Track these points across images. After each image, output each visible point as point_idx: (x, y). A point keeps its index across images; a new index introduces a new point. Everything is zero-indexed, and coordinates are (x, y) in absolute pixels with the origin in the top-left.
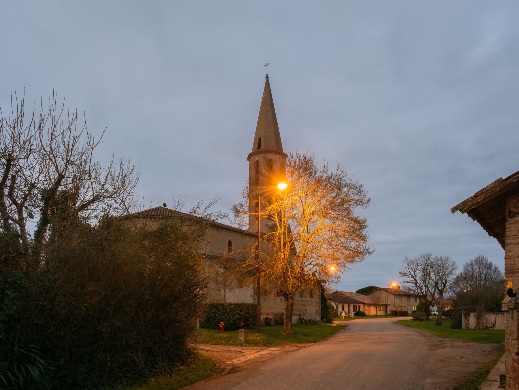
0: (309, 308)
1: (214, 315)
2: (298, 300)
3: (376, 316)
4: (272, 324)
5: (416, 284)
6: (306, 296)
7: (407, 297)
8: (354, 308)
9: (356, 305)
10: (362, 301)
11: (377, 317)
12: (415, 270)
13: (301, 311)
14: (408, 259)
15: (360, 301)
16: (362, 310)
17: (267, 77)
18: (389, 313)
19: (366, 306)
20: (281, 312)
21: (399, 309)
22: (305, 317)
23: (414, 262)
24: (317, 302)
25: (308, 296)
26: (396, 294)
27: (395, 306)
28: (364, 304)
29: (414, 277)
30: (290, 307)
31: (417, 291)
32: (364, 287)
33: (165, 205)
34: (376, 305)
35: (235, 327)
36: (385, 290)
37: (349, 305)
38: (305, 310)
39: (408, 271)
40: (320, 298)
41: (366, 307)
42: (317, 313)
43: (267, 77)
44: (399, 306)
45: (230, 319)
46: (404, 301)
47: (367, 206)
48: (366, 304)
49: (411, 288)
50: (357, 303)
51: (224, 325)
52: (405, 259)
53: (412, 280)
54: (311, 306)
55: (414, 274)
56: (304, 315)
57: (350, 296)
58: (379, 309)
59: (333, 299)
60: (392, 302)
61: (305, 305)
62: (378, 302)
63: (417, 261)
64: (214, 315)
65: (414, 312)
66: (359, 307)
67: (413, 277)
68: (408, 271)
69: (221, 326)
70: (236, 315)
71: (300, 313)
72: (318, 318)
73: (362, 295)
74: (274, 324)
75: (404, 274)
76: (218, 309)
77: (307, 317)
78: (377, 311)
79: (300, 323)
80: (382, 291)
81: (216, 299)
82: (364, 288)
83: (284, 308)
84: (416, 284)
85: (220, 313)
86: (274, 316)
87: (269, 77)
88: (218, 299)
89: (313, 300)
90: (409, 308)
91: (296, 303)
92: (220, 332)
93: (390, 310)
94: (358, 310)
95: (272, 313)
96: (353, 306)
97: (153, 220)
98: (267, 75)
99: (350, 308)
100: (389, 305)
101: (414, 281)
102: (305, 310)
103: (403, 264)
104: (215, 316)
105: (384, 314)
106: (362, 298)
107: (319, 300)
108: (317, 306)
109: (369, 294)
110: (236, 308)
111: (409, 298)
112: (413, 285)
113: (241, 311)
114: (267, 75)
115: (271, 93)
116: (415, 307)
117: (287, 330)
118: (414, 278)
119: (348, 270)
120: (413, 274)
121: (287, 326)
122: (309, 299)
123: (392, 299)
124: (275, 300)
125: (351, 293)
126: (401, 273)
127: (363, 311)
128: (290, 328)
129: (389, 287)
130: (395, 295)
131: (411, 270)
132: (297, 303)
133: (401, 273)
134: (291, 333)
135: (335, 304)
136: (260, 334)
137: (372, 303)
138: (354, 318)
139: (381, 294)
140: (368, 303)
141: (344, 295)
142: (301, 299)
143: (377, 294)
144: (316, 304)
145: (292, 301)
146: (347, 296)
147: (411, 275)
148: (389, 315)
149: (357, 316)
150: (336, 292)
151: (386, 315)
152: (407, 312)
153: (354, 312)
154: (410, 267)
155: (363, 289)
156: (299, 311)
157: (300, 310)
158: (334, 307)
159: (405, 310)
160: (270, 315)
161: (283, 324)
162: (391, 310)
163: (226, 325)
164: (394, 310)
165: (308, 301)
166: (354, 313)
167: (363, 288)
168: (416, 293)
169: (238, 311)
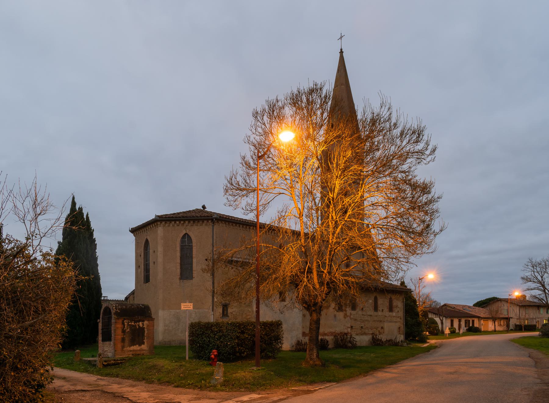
0: (386, 325)
1: (209, 339)
2: (371, 316)
3: (495, 332)
4: (330, 346)
5: (544, 291)
6: (382, 310)
7: (535, 308)
8: (466, 323)
9: (469, 319)
10: (476, 314)
11: (496, 333)
12: (543, 273)
13: (375, 330)
14: (534, 260)
15: (475, 314)
16: (476, 325)
17: (341, 52)
18: (511, 327)
19: (482, 321)
20: (346, 331)
21: (525, 322)
22: (379, 337)
23: (540, 264)
24: (399, 317)
25: (386, 309)
26: (521, 305)
27: (519, 318)
28: (479, 318)
29: (541, 282)
30: (314, 324)
31: (546, 301)
32: (483, 298)
33: (204, 207)
34: (494, 319)
35: (234, 357)
36: (506, 301)
37: (459, 320)
38: (382, 327)
39: (533, 275)
40: (404, 312)
41: (482, 322)
42: (399, 331)
43: (341, 52)
44: (524, 319)
45: (227, 346)
46: (532, 313)
47: (433, 159)
48: (482, 318)
49: (538, 296)
50: (470, 317)
51: (216, 354)
52: (529, 261)
53: (539, 286)
54: (391, 322)
55: (542, 278)
56: (380, 333)
57: (461, 309)
58: (498, 323)
59: (437, 313)
60: (516, 315)
61: (381, 322)
62: (496, 314)
63: (545, 263)
64: (209, 339)
65: (544, 325)
66: (473, 321)
67: (540, 283)
68: (533, 275)
69: (213, 356)
70: (235, 339)
71: (374, 332)
72: (401, 338)
73: (477, 308)
74: (333, 348)
75: (526, 279)
76: (212, 332)
77: (384, 338)
78: (495, 326)
79: (373, 345)
80: (503, 302)
81: (248, 317)
82: (483, 300)
83: (349, 326)
84: (544, 291)
85: (214, 337)
86: (335, 336)
87: (343, 52)
88: (249, 317)
89: (394, 314)
90: (538, 321)
91: (367, 319)
92: (212, 365)
93: (513, 324)
94: (471, 325)
95: (332, 334)
96: (465, 320)
97: (178, 222)
98: (341, 50)
99: (461, 323)
100: (511, 318)
101: (542, 288)
102: (382, 328)
103: (526, 267)
104: (209, 341)
105: (505, 329)
106: (482, 312)
107: (402, 315)
108: (400, 322)
109: (486, 306)
110: (234, 328)
111: (538, 309)
112: (540, 292)
113: (243, 333)
114: (341, 50)
115: (346, 70)
116: (546, 320)
117: (311, 359)
118: (541, 284)
119: (412, 265)
120: (540, 279)
121: (311, 354)
122: (387, 314)
123: (515, 311)
124: (335, 316)
125: (469, 307)
126: (523, 278)
127: (478, 326)
128: (315, 356)
129: (510, 297)
130: (520, 306)
131: (536, 274)
132: (369, 319)
133: (523, 278)
134: (316, 365)
135: (440, 319)
136: (258, 368)
137: (488, 316)
138: (464, 335)
139: (502, 306)
140: (484, 316)
141: (454, 308)
142: (376, 313)
143: (494, 307)
144: (399, 320)
145: (317, 316)
146: (458, 309)
147: (536, 280)
148: (512, 330)
149: (470, 332)
150: (445, 305)
151: (508, 331)
152: (535, 326)
153: (467, 328)
154: (535, 270)
155: (482, 301)
156: (372, 329)
157: (374, 328)
158: (438, 322)
159: (533, 324)
160: (328, 335)
161: (306, 351)
162: (515, 324)
163: (219, 353)
164: (518, 323)
165: (386, 316)
166: (467, 329)
167: (482, 300)
168: (545, 303)
169: (238, 333)
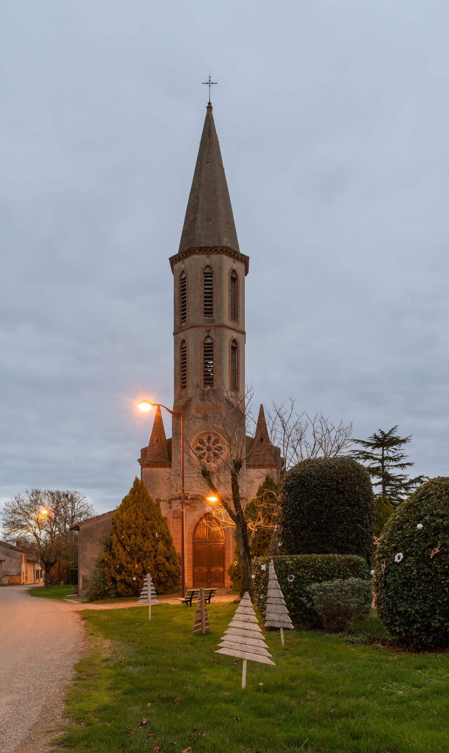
17: (210, 108)
43: (210, 108)
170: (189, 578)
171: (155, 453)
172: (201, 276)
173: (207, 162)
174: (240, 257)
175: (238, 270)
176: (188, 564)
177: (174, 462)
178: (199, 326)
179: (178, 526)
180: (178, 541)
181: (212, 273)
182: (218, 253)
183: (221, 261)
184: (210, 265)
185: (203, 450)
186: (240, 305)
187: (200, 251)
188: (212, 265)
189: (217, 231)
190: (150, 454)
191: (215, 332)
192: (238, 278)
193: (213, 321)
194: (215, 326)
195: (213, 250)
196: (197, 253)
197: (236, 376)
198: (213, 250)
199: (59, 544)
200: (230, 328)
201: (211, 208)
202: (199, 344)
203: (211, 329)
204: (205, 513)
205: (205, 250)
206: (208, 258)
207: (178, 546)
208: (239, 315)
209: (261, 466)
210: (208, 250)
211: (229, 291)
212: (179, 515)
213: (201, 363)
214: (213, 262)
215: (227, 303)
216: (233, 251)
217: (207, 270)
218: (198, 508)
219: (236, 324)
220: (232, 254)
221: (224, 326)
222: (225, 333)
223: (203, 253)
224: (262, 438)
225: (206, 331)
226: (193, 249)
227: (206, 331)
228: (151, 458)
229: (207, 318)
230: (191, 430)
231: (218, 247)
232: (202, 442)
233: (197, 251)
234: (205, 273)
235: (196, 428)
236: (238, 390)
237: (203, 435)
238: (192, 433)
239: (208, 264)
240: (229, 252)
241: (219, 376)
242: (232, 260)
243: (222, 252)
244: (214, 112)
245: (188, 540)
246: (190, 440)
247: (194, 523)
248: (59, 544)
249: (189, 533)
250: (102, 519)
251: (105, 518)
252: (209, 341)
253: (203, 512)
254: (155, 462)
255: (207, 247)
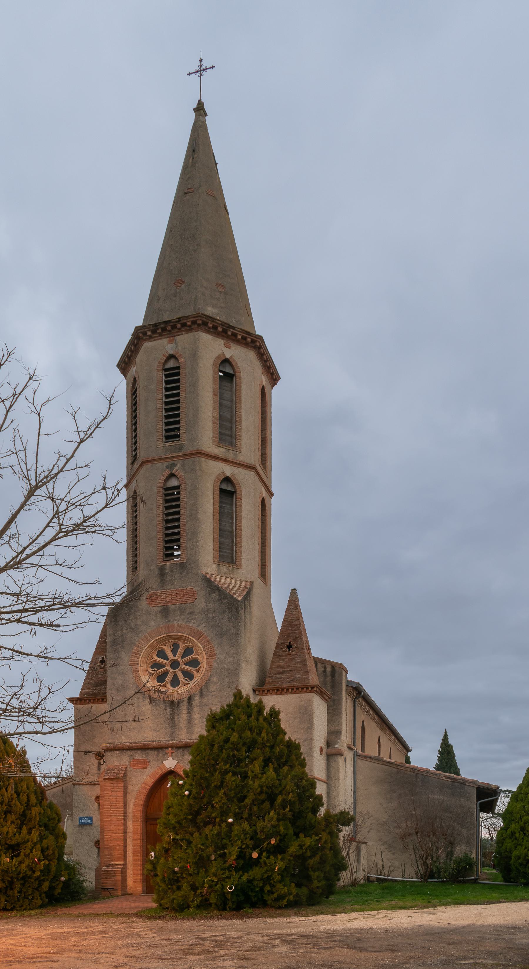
17: (200, 110)
43: (200, 110)
170: (135, 878)
171: (97, 681)
172: (159, 376)
173: (186, 193)
174: (239, 337)
175: (236, 359)
176: (134, 856)
177: (111, 689)
178: (154, 460)
179: (113, 793)
180: (114, 819)
181: (178, 368)
182: (190, 329)
183: (195, 342)
184: (174, 354)
185: (165, 667)
186: (243, 419)
187: (154, 332)
188: (177, 353)
189: (193, 297)
190: (88, 684)
191: (183, 466)
192: (237, 374)
193: (181, 448)
194: (184, 455)
195: (179, 326)
196: (150, 338)
197: (233, 541)
198: (179, 326)
199: (165, 824)
200: (215, 458)
201: (186, 262)
202: (155, 489)
203: (175, 463)
204: (164, 771)
205: (164, 330)
206: (170, 342)
207: (113, 826)
208: (240, 436)
209: (283, 690)
210: (169, 328)
211: (214, 394)
212: (114, 776)
213: (159, 521)
214: (180, 348)
215: (210, 414)
216: (222, 325)
217: (171, 364)
218: (152, 763)
219: (231, 451)
220: (220, 329)
221: (200, 454)
222: (204, 466)
223: (161, 335)
224: (290, 643)
225: (167, 467)
226: (142, 331)
227: (167, 467)
228: (89, 689)
229: (170, 444)
230: (140, 635)
231: (187, 317)
232: (162, 654)
233: (149, 333)
234: (166, 370)
235: (149, 631)
236: (238, 563)
237: (163, 641)
238: (143, 640)
239: (171, 352)
240: (210, 325)
241: (190, 540)
242: (221, 342)
243: (196, 326)
244: (208, 120)
245: (134, 816)
246: (139, 651)
247: (144, 788)
248: (165, 824)
249: (135, 805)
250: (54, 790)
251: (57, 788)
252: (174, 482)
253: (161, 769)
254: (96, 695)
255: (166, 322)
